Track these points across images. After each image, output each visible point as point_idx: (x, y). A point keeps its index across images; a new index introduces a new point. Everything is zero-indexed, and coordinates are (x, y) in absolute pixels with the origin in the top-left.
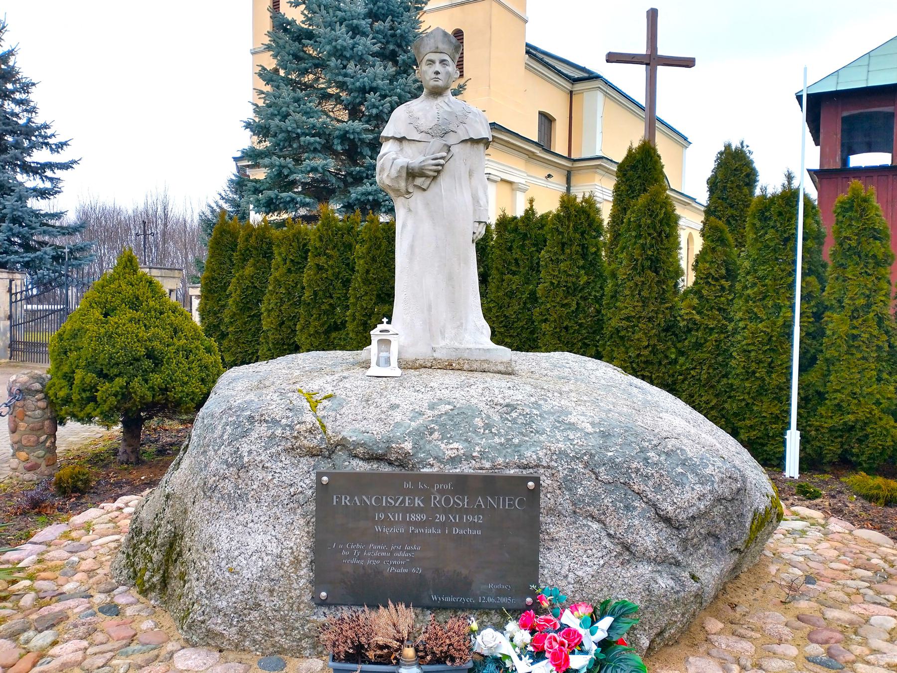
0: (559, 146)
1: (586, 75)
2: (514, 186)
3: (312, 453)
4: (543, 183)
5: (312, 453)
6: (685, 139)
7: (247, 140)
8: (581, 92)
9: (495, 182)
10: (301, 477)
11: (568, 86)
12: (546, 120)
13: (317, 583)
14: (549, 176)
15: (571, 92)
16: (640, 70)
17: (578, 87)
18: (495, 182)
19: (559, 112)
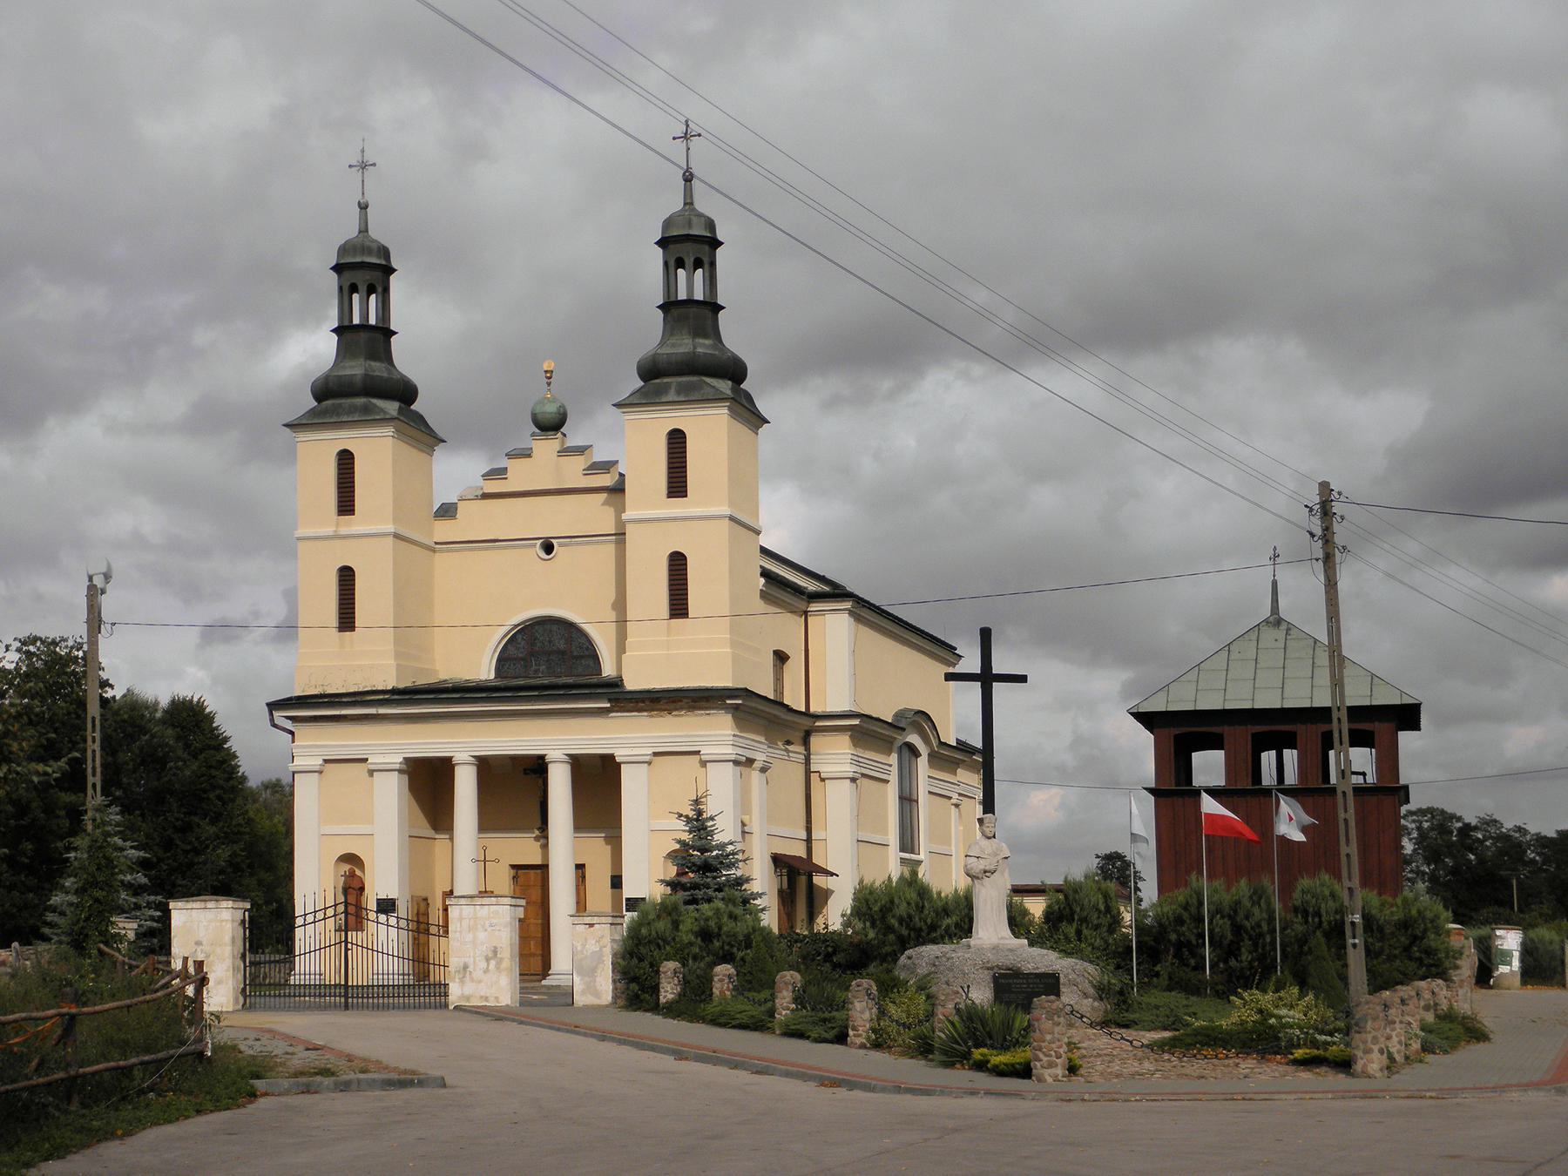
16: (997, 669)
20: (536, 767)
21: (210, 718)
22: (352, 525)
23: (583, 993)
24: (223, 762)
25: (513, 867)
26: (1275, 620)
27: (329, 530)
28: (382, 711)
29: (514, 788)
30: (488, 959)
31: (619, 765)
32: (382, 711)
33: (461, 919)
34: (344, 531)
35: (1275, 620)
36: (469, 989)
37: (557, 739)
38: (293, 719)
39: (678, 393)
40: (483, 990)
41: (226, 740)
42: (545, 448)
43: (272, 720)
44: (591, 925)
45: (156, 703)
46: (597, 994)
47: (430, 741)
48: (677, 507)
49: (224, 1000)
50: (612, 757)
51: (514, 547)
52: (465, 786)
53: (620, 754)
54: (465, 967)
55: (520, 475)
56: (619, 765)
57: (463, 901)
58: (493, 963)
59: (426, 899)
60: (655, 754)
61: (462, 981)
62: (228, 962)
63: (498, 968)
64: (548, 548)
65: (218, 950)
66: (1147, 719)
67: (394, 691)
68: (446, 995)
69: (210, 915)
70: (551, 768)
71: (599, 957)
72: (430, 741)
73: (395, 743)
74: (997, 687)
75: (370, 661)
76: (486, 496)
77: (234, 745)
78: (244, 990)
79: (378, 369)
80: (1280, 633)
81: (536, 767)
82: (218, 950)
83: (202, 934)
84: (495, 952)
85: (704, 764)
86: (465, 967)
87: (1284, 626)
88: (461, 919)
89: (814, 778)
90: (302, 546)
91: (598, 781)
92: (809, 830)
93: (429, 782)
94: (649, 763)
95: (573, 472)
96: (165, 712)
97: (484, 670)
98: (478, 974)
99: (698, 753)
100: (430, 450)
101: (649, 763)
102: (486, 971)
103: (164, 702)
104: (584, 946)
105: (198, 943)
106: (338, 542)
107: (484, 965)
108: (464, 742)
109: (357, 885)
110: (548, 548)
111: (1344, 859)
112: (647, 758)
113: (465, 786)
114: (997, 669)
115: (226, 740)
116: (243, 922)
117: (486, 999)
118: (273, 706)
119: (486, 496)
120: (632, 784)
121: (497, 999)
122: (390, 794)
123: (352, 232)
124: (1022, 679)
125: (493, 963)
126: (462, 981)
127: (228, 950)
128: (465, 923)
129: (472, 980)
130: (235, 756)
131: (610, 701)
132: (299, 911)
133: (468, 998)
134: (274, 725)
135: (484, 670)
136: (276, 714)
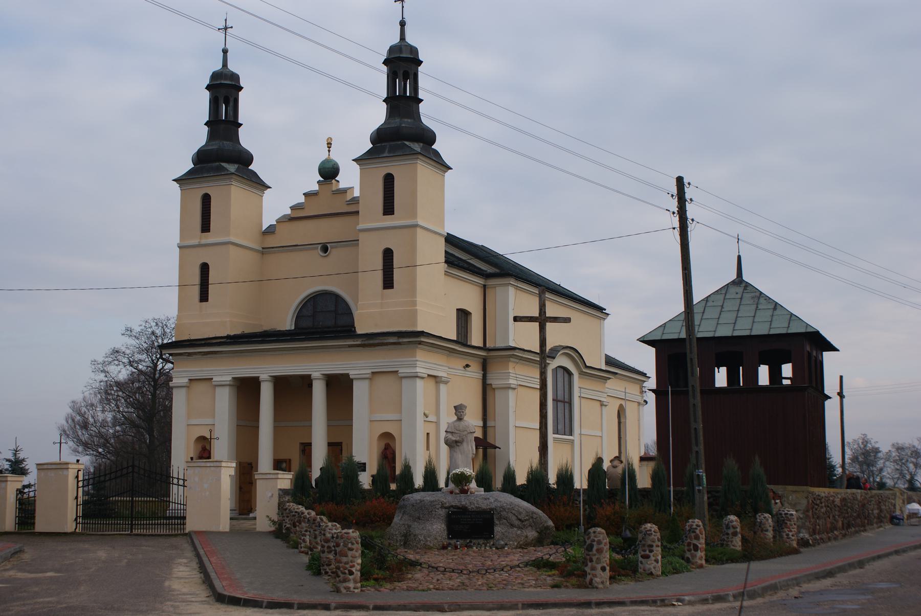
0: (476, 339)
1: (498, 271)
2: (438, 380)
3: (446, 508)
4: (461, 372)
5: (446, 508)
6: (601, 309)
7: (126, 343)
8: (494, 287)
9: (423, 378)
10: (443, 512)
11: (481, 281)
12: (463, 315)
13: (448, 535)
14: (467, 366)
15: (485, 286)
16: (549, 314)
17: (491, 282)
18: (423, 378)
19: (472, 304)
20: (306, 381)
22: (209, 238)
25: (302, 444)
26: (739, 280)
27: (195, 242)
31: (352, 380)
34: (203, 241)
35: (739, 280)
37: (316, 364)
39: (389, 152)
47: (246, 368)
48: (389, 221)
50: (348, 375)
51: (307, 250)
52: (267, 393)
53: (352, 373)
56: (352, 380)
59: (250, 464)
64: (325, 249)
66: (646, 341)
67: (228, 337)
68: (184, 524)
70: (357, 386)
73: (225, 371)
74: (549, 326)
75: (220, 318)
78: (76, 519)
79: (227, 145)
80: (740, 290)
81: (306, 381)
87: (744, 285)
89: (488, 388)
91: (340, 388)
92: (485, 420)
93: (247, 389)
94: (370, 379)
97: (287, 323)
100: (263, 191)
101: (370, 379)
108: (266, 368)
111: (693, 431)
112: (367, 376)
113: (267, 393)
114: (549, 314)
120: (360, 391)
123: (218, 66)
124: (841, 377)
135: (287, 323)
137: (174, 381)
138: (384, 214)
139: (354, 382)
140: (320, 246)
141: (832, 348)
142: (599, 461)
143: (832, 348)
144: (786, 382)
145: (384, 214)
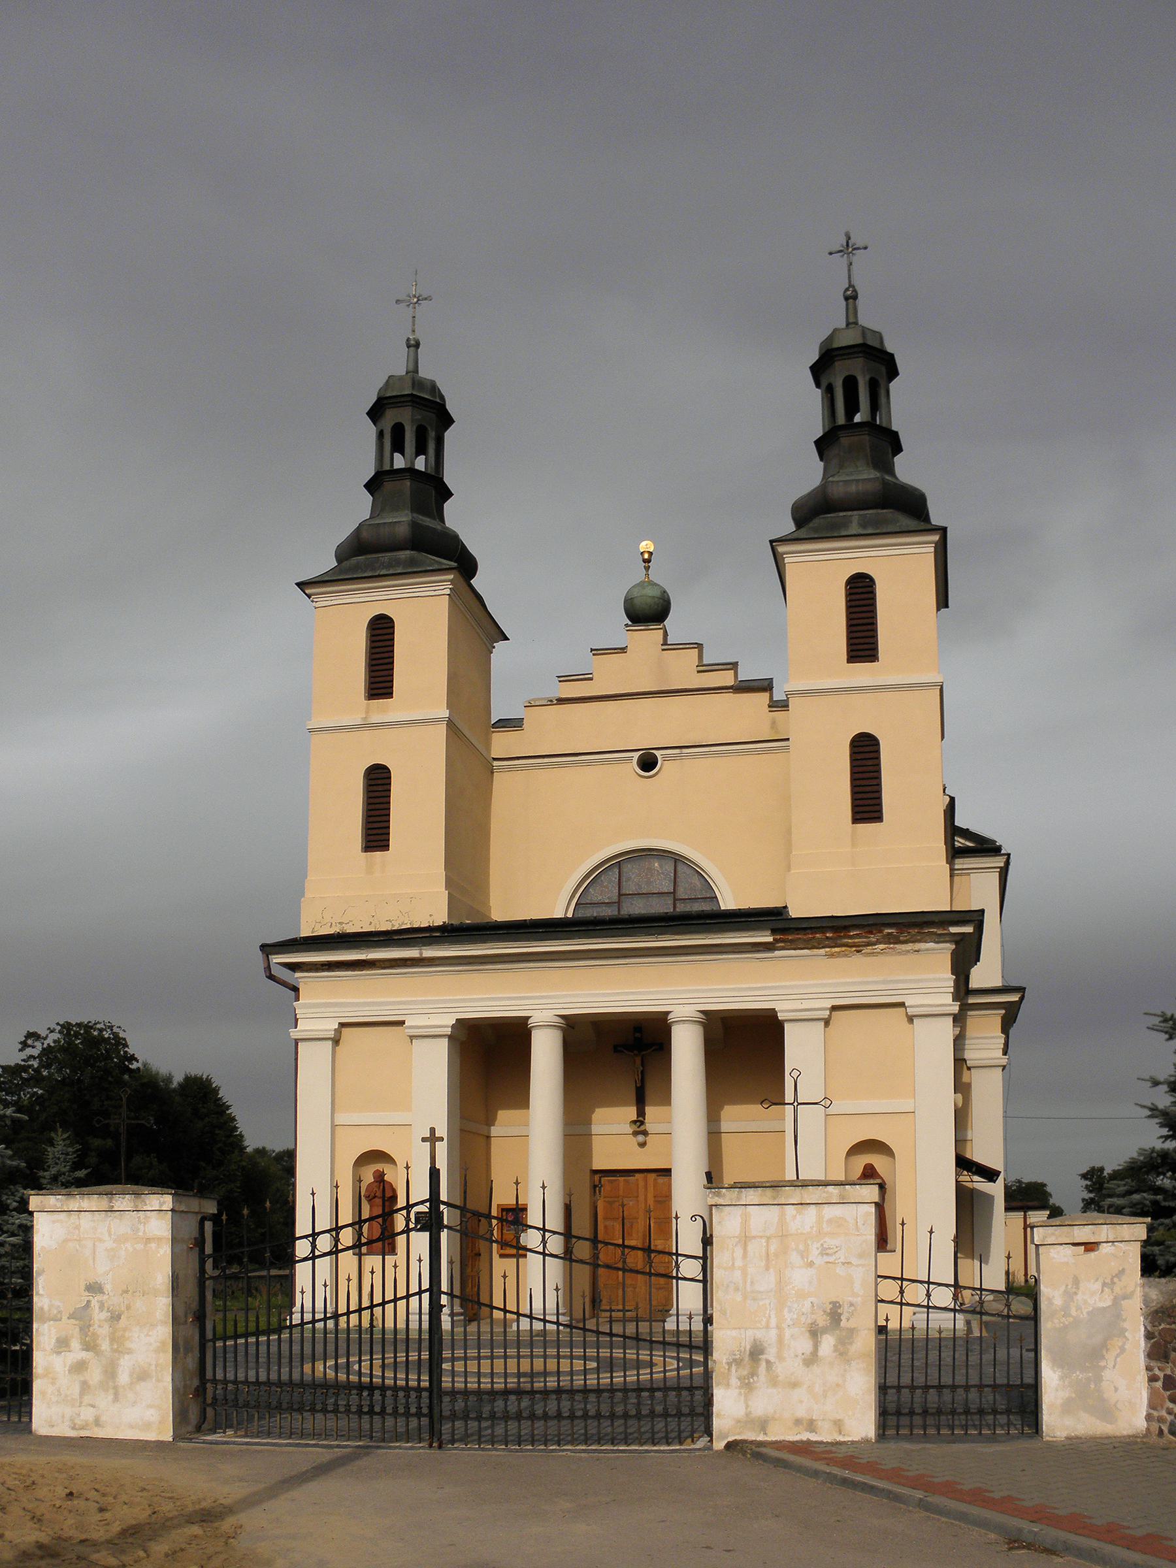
8: (967, 871)
21: (216, 1091)
22: (384, 711)
23: (1067, 1408)
24: (225, 1123)
28: (429, 952)
29: (619, 1054)
30: (815, 1333)
32: (429, 952)
33: (745, 1239)
34: (376, 718)
36: (764, 1402)
37: (682, 990)
38: (294, 967)
39: (864, 526)
40: (802, 1404)
41: (228, 1107)
42: (648, 638)
43: (268, 968)
44: (1090, 1247)
45: (169, 1079)
46: (1105, 1411)
47: (492, 995)
48: (863, 674)
49: (152, 1415)
52: (546, 1055)
53: (783, 1010)
54: (756, 1352)
55: (609, 676)
57: (751, 1196)
58: (828, 1343)
60: (834, 1008)
61: (747, 1385)
62: (163, 1332)
63: (842, 1351)
64: (648, 763)
65: (139, 1304)
67: (443, 929)
69: (120, 1225)
70: (793, 1037)
71: (1111, 1320)
72: (492, 995)
76: (561, 701)
77: (226, 1094)
82: (139, 1304)
83: (102, 1270)
84: (835, 1314)
85: (911, 1019)
86: (756, 1352)
88: (745, 1239)
90: (316, 738)
93: (490, 1057)
95: (682, 669)
96: (180, 1085)
98: (790, 1367)
99: (902, 1005)
102: (811, 1360)
103: (178, 1078)
104: (1069, 1296)
105: (94, 1288)
106: (366, 735)
107: (805, 1345)
108: (547, 997)
109: (388, 1194)
110: (648, 763)
113: (546, 1055)
115: (228, 1107)
116: (200, 1242)
117: (811, 1425)
118: (268, 949)
119: (561, 701)
120: (801, 1049)
121: (838, 1425)
122: (430, 1076)
125: (828, 1343)
126: (747, 1385)
127: (162, 1305)
128: (755, 1248)
129: (774, 1382)
130: (234, 1119)
131: (774, 931)
132: (302, 1226)
133: (763, 1425)
134: (271, 977)
136: (277, 959)
137: (301, 1025)
138: (855, 820)
139: (786, 1026)
140: (636, 755)
141: (1168, 1040)
142: (1154, 1112)
143: (1168, 1040)
144: (4, 1197)
145: (855, 820)
